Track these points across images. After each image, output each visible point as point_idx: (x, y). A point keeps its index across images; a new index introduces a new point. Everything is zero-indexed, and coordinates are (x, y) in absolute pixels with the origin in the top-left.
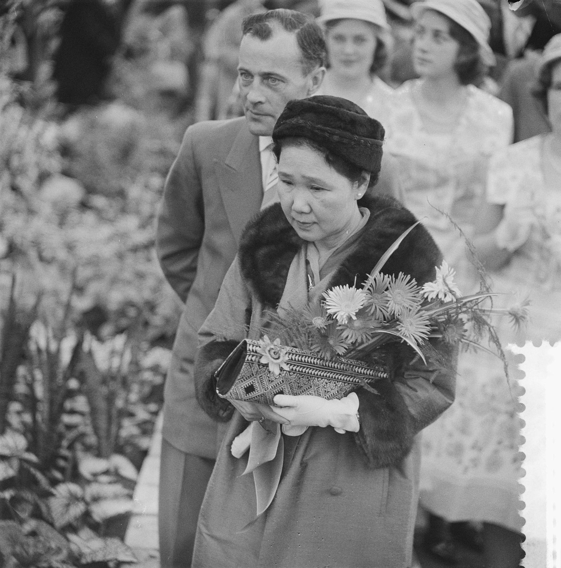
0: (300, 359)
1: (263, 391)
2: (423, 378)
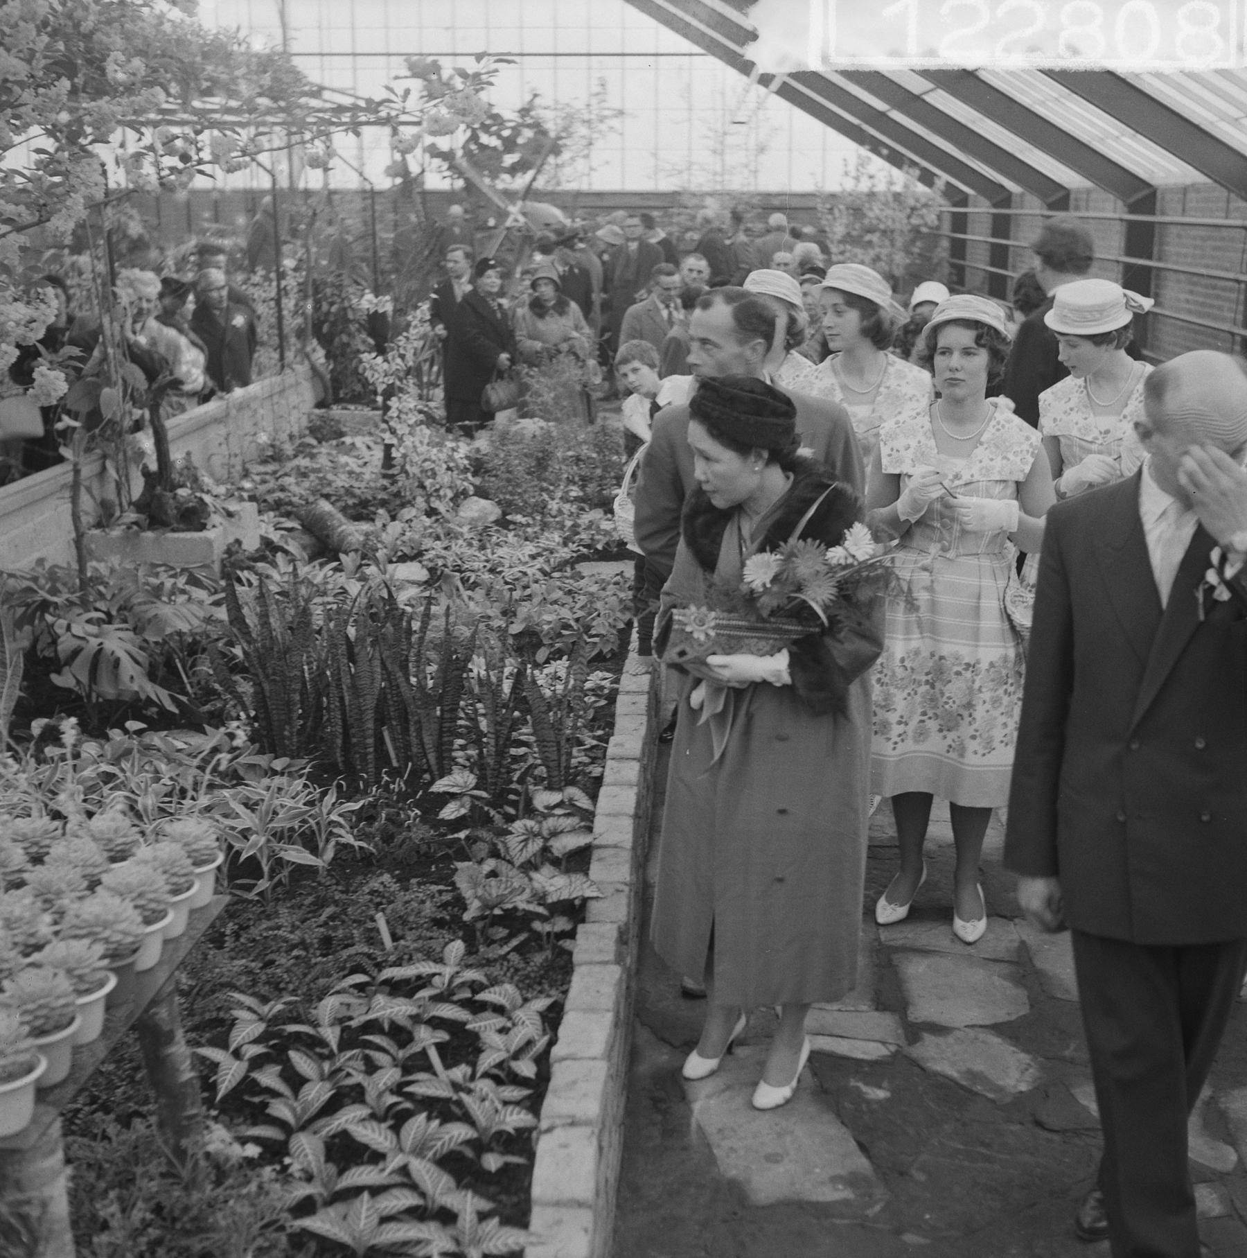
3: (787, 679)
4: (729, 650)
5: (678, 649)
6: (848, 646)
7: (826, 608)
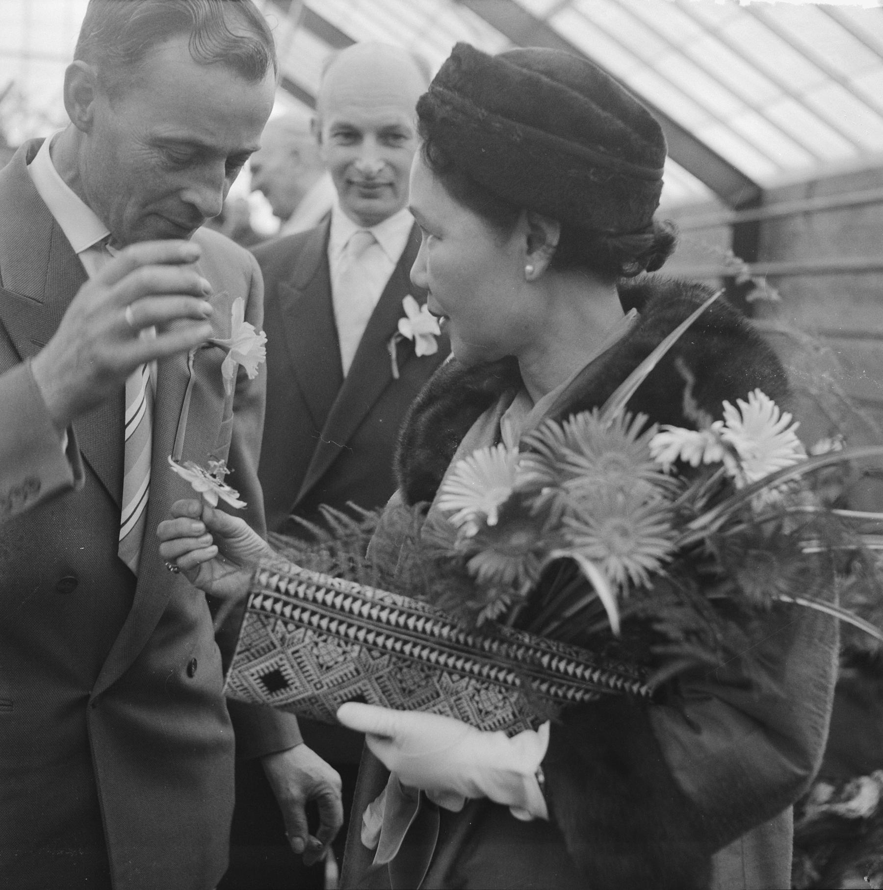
0: (402, 620)
1: (310, 692)
2: (721, 700)
3: (535, 803)
4: (403, 698)
5: (265, 665)
6: (711, 741)
7: (628, 591)
